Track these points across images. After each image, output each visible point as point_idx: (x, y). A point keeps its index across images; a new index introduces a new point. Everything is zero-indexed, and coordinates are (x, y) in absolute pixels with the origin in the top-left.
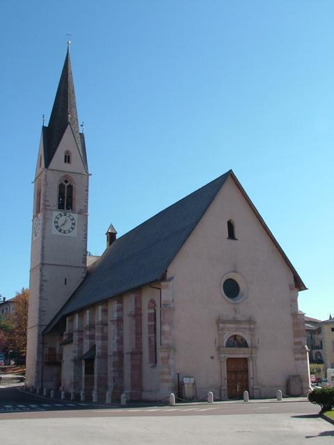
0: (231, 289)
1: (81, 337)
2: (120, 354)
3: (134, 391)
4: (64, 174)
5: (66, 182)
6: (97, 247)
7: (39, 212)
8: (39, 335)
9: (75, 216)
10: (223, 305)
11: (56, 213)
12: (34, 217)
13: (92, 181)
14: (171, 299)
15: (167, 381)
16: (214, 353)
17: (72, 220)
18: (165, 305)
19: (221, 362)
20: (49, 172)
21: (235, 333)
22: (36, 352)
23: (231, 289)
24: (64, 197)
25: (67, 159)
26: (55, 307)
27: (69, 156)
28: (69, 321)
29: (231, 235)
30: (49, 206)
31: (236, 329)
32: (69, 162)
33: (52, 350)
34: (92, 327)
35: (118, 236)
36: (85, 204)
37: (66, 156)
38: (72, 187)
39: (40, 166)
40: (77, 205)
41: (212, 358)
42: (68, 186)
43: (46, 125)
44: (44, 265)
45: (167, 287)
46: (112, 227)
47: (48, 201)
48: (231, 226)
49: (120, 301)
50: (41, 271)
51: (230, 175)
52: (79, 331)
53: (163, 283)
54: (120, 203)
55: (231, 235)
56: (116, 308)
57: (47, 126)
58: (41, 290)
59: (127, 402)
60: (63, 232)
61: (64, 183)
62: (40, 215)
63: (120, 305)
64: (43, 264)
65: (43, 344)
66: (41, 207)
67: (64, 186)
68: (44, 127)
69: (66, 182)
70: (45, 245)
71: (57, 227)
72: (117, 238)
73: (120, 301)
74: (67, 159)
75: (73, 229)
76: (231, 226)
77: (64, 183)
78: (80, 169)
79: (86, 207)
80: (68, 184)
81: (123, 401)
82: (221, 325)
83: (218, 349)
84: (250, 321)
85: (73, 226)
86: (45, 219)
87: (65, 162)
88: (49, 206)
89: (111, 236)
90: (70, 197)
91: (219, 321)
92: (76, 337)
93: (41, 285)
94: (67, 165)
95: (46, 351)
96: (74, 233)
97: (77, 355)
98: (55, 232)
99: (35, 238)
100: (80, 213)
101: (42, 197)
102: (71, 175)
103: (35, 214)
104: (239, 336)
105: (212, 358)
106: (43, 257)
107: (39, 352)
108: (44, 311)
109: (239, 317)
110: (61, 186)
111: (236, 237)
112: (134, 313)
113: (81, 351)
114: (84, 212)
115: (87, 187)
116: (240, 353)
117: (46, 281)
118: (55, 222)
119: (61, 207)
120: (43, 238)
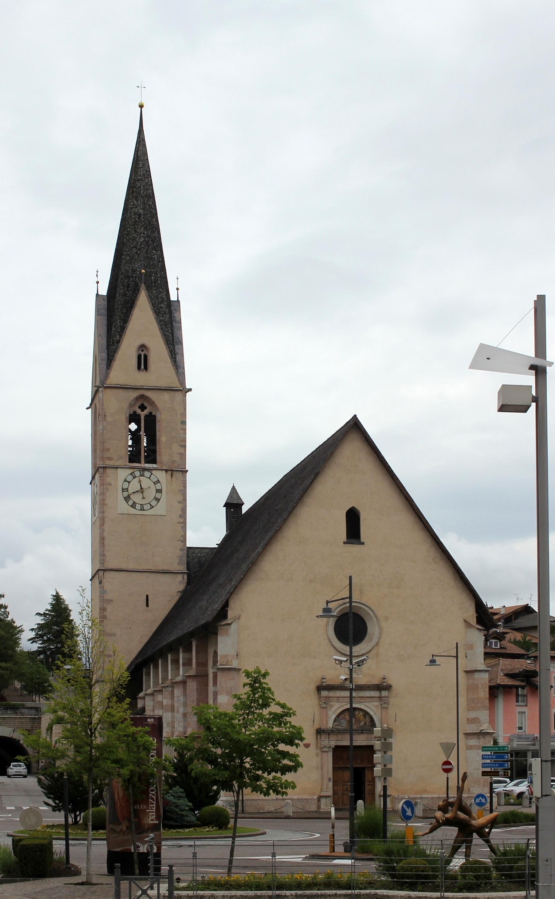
4: (135, 394)
5: (143, 408)
14: (233, 652)
17: (155, 483)
23: (351, 627)
24: (140, 431)
25: (143, 362)
27: (146, 357)
29: (353, 532)
32: (146, 368)
36: (182, 451)
37: (139, 357)
38: (155, 416)
42: (146, 416)
43: (104, 291)
47: (108, 450)
48: (353, 519)
51: (354, 426)
55: (353, 532)
57: (105, 293)
60: (138, 507)
61: (139, 411)
67: (139, 416)
68: (97, 295)
70: (106, 534)
71: (127, 499)
72: (243, 512)
74: (143, 362)
75: (158, 500)
76: (353, 519)
77: (139, 411)
78: (171, 380)
80: (146, 412)
82: (324, 693)
87: (139, 368)
88: (110, 459)
94: (143, 374)
96: (160, 509)
98: (124, 507)
99: (94, 519)
100: (171, 471)
102: (149, 394)
104: (366, 713)
106: (103, 556)
111: (362, 540)
113: (185, 733)
114: (178, 471)
118: (123, 490)
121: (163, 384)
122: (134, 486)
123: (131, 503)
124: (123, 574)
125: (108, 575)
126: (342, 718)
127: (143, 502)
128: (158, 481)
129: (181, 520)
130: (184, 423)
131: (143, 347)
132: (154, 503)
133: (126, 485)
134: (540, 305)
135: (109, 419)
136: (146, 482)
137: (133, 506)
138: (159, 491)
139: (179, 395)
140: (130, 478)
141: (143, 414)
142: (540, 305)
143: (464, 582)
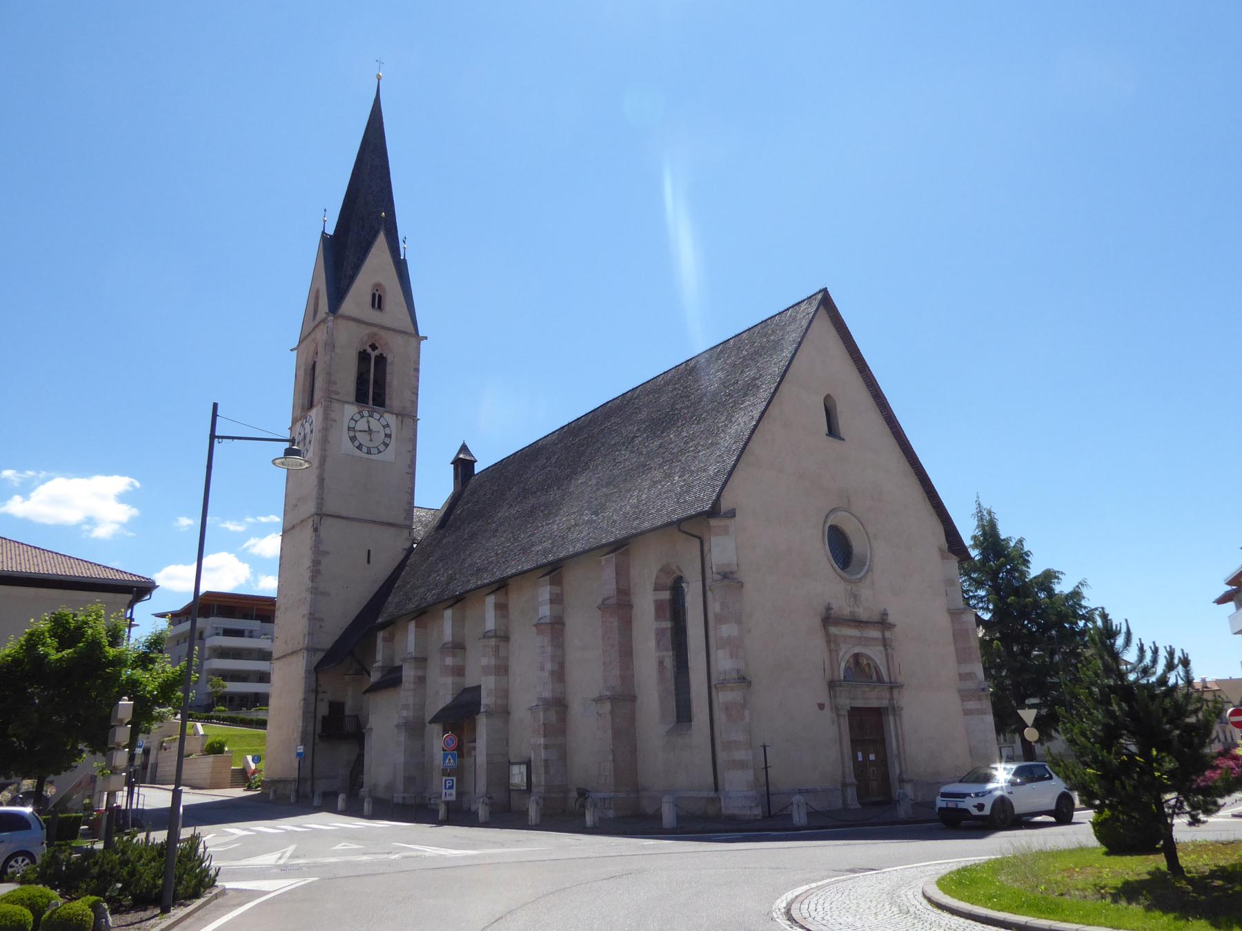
0: (841, 548)
1: (420, 673)
2: (622, 699)
3: (620, 795)
6: (433, 490)
7: (311, 405)
8: (308, 672)
9: (390, 419)
10: (828, 586)
11: (351, 410)
12: (294, 421)
13: (428, 354)
15: (741, 765)
16: (824, 697)
17: (386, 435)
18: (726, 576)
19: (838, 715)
20: (342, 323)
21: (857, 650)
22: (300, 713)
23: (841, 548)
25: (378, 302)
26: (343, 609)
27: (380, 297)
28: (385, 639)
30: (337, 393)
31: (862, 641)
32: (379, 307)
33: (336, 708)
34: (458, 647)
35: (478, 468)
37: (374, 295)
39: (316, 312)
40: (394, 397)
41: (821, 706)
43: (331, 230)
44: (314, 522)
45: (726, 531)
46: (464, 448)
49: (557, 581)
50: (316, 530)
52: (416, 659)
53: (714, 522)
54: (483, 399)
55: (832, 430)
56: (547, 597)
58: (316, 573)
59: (679, 818)
60: (364, 449)
61: (369, 350)
62: (315, 414)
63: (557, 589)
64: (321, 515)
65: (317, 692)
66: (318, 395)
69: (374, 347)
71: (353, 439)
73: (557, 581)
74: (378, 302)
75: (386, 445)
78: (403, 322)
79: (414, 404)
80: (377, 352)
81: (589, 819)
83: (832, 685)
84: (883, 623)
85: (387, 440)
86: (328, 421)
87: (373, 306)
89: (463, 466)
90: (381, 384)
91: (829, 619)
92: (409, 673)
93: (316, 563)
95: (323, 710)
96: (389, 455)
97: (411, 714)
101: (319, 384)
103: (299, 413)
104: (868, 658)
105: (821, 706)
107: (305, 713)
108: (321, 620)
109: (863, 614)
110: (363, 357)
112: (613, 601)
114: (409, 416)
115: (417, 363)
116: (872, 698)
117: (327, 553)
118: (349, 429)
119: (361, 398)
120: (323, 460)
121: (395, 325)
122: (362, 425)
123: (357, 444)
124: (343, 521)
125: (328, 522)
126: (202, 659)
127: (370, 444)
128: (388, 425)
129: (410, 470)
130: (417, 370)
131: (378, 286)
132: (382, 448)
133: (352, 424)
134: (215, 406)
135: (337, 350)
136: (375, 425)
137: (360, 447)
138: (388, 436)
139: (413, 340)
140: (357, 417)
141: (373, 354)
142: (215, 406)
143: (891, 429)
